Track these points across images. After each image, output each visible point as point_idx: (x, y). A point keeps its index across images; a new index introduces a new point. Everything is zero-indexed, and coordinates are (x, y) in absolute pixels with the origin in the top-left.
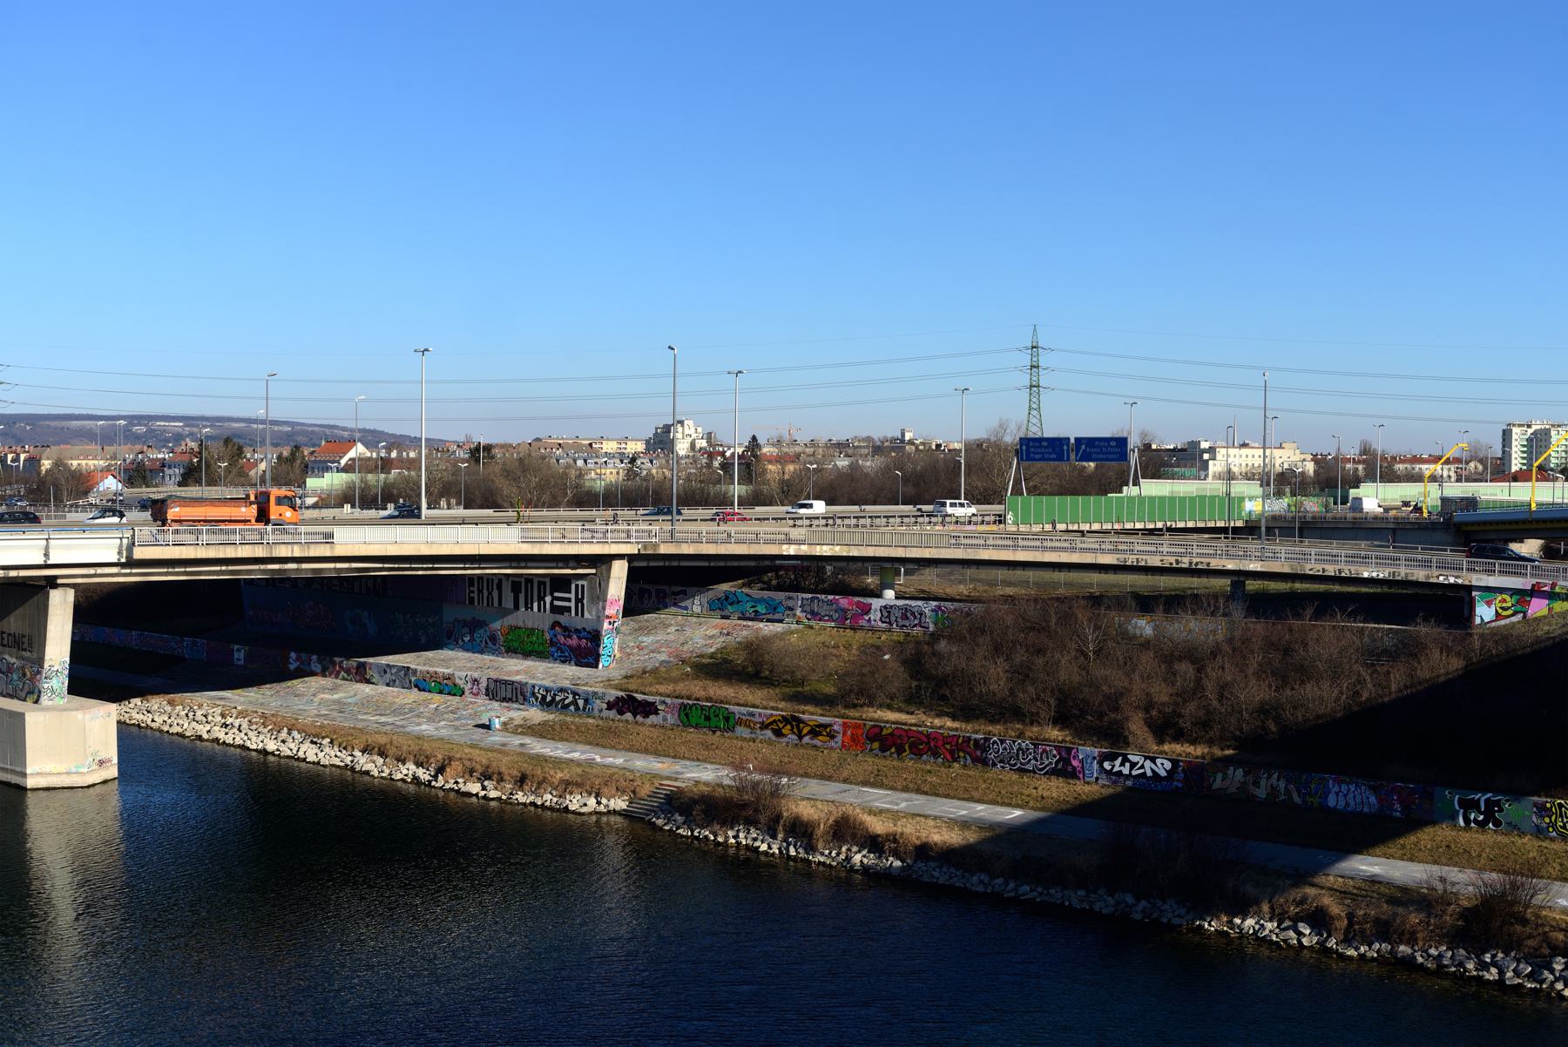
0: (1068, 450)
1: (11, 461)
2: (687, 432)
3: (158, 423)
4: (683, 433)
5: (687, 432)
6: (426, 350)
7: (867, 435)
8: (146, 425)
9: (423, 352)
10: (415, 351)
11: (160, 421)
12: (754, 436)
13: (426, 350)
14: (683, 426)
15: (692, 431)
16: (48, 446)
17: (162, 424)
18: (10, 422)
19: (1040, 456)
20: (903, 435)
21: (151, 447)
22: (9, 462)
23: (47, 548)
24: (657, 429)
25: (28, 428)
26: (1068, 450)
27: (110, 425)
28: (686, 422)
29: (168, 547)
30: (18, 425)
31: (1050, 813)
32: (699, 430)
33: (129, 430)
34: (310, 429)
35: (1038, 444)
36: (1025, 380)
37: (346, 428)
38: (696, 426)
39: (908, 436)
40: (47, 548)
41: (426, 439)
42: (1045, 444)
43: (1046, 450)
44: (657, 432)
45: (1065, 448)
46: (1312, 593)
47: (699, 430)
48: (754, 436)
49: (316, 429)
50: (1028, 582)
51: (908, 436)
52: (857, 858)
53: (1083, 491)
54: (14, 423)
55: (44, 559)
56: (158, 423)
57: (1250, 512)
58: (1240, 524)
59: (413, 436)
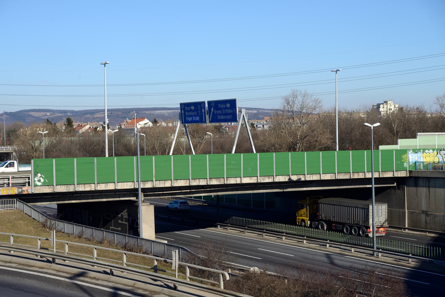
1: (13, 163)
6: (338, 70)
7: (7, 111)
9: (336, 71)
13: (338, 70)
14: (387, 104)
18: (128, 112)
22: (15, 162)
24: (373, 106)
28: (389, 102)
29: (26, 213)
30: (131, 113)
31: (77, 278)
34: (266, 111)
41: (437, 145)
45: (203, 111)
49: (269, 111)
52: (217, 124)
54: (129, 112)
57: (415, 162)
58: (402, 174)
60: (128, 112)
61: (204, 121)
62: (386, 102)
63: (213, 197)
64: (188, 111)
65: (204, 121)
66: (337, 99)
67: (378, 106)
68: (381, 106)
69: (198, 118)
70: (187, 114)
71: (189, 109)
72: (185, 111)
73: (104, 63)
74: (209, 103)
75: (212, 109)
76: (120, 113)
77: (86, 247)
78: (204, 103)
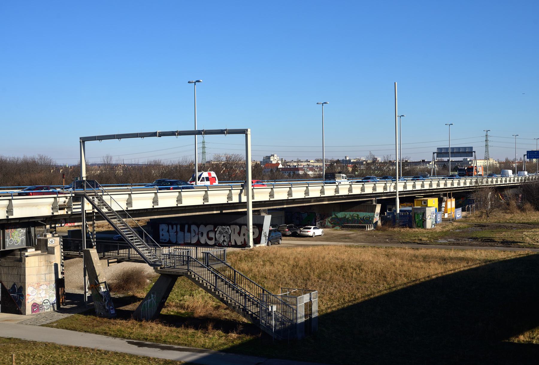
4: (274, 159)
19: (533, 157)
24: (264, 157)
35: (533, 153)
44: (264, 159)
51: (348, 159)
61: (523, 170)
62: (273, 155)
65: (523, 170)
67: (268, 158)
68: (271, 157)
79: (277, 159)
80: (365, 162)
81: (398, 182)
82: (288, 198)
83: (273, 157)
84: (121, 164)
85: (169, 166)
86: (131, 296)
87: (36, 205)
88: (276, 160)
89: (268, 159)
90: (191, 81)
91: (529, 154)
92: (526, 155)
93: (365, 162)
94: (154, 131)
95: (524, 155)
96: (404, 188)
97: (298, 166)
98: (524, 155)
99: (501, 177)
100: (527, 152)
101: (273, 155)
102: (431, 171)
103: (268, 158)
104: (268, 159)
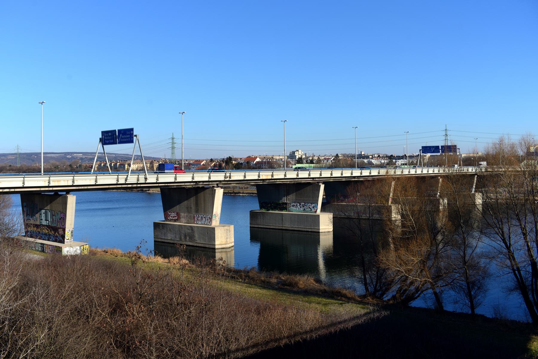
0: (116, 137)
2: (299, 153)
3: (75, 155)
4: (298, 154)
5: (299, 153)
6: (184, 113)
8: (70, 155)
10: (281, 121)
11: (75, 154)
12: (337, 154)
13: (184, 113)
15: (301, 153)
16: (126, 161)
17: (76, 155)
20: (361, 153)
21: (155, 160)
23: (96, 179)
24: (290, 153)
25: (36, 157)
26: (116, 137)
27: (59, 155)
30: (32, 156)
32: (303, 153)
33: (66, 157)
36: (444, 138)
37: (34, 157)
38: (302, 151)
39: (363, 153)
40: (96, 179)
42: (428, 148)
43: (429, 150)
44: (290, 153)
46: (289, 184)
47: (303, 153)
48: (337, 154)
50: (312, 167)
51: (363, 153)
53: (51, 245)
54: (31, 155)
55: (48, 184)
56: (75, 155)
59: (153, 157)
60: (30, 155)
61: (115, 142)
62: (298, 151)
63: (235, 169)
64: (107, 136)
65: (115, 142)
66: (183, 143)
67: (294, 153)
68: (296, 152)
69: (112, 141)
70: (105, 138)
71: (107, 135)
72: (104, 136)
73: (42, 102)
74: (119, 131)
75: (121, 135)
76: (25, 156)
77: (279, 170)
78: (115, 131)
79: (301, 154)
80: (371, 156)
81: (129, 174)
82: (125, 182)
83: (298, 153)
84: (163, 158)
85: (224, 159)
86: (515, 276)
87: (12, 181)
88: (300, 154)
89: (293, 153)
90: (180, 112)
91: (423, 149)
92: (421, 150)
93: (371, 156)
94: (27, 148)
95: (420, 150)
96: (209, 178)
97: (272, 160)
98: (420, 150)
99: (175, 172)
100: (422, 147)
101: (298, 151)
102: (355, 165)
103: (294, 153)
104: (293, 153)
